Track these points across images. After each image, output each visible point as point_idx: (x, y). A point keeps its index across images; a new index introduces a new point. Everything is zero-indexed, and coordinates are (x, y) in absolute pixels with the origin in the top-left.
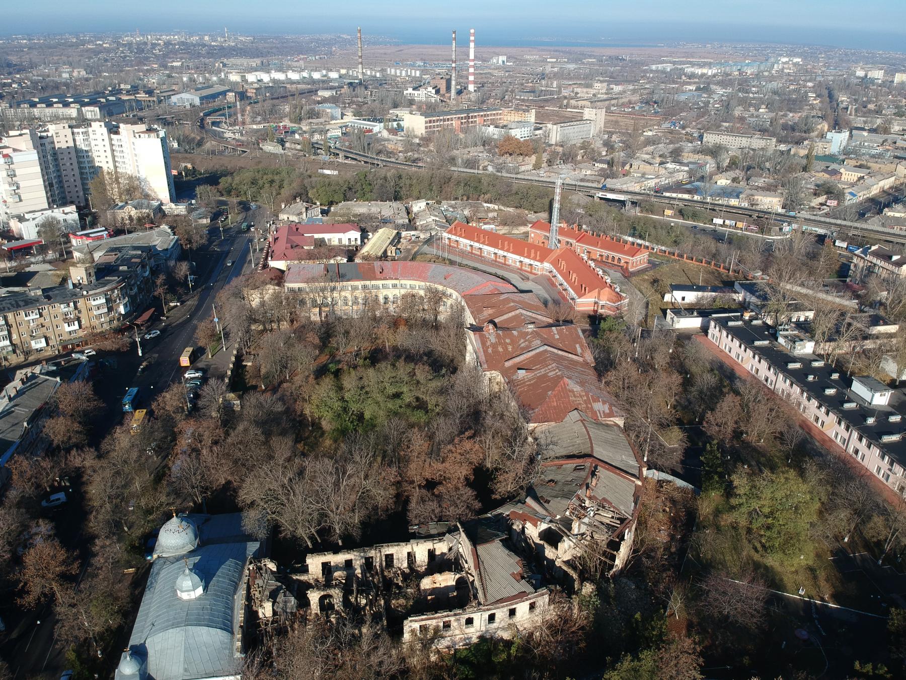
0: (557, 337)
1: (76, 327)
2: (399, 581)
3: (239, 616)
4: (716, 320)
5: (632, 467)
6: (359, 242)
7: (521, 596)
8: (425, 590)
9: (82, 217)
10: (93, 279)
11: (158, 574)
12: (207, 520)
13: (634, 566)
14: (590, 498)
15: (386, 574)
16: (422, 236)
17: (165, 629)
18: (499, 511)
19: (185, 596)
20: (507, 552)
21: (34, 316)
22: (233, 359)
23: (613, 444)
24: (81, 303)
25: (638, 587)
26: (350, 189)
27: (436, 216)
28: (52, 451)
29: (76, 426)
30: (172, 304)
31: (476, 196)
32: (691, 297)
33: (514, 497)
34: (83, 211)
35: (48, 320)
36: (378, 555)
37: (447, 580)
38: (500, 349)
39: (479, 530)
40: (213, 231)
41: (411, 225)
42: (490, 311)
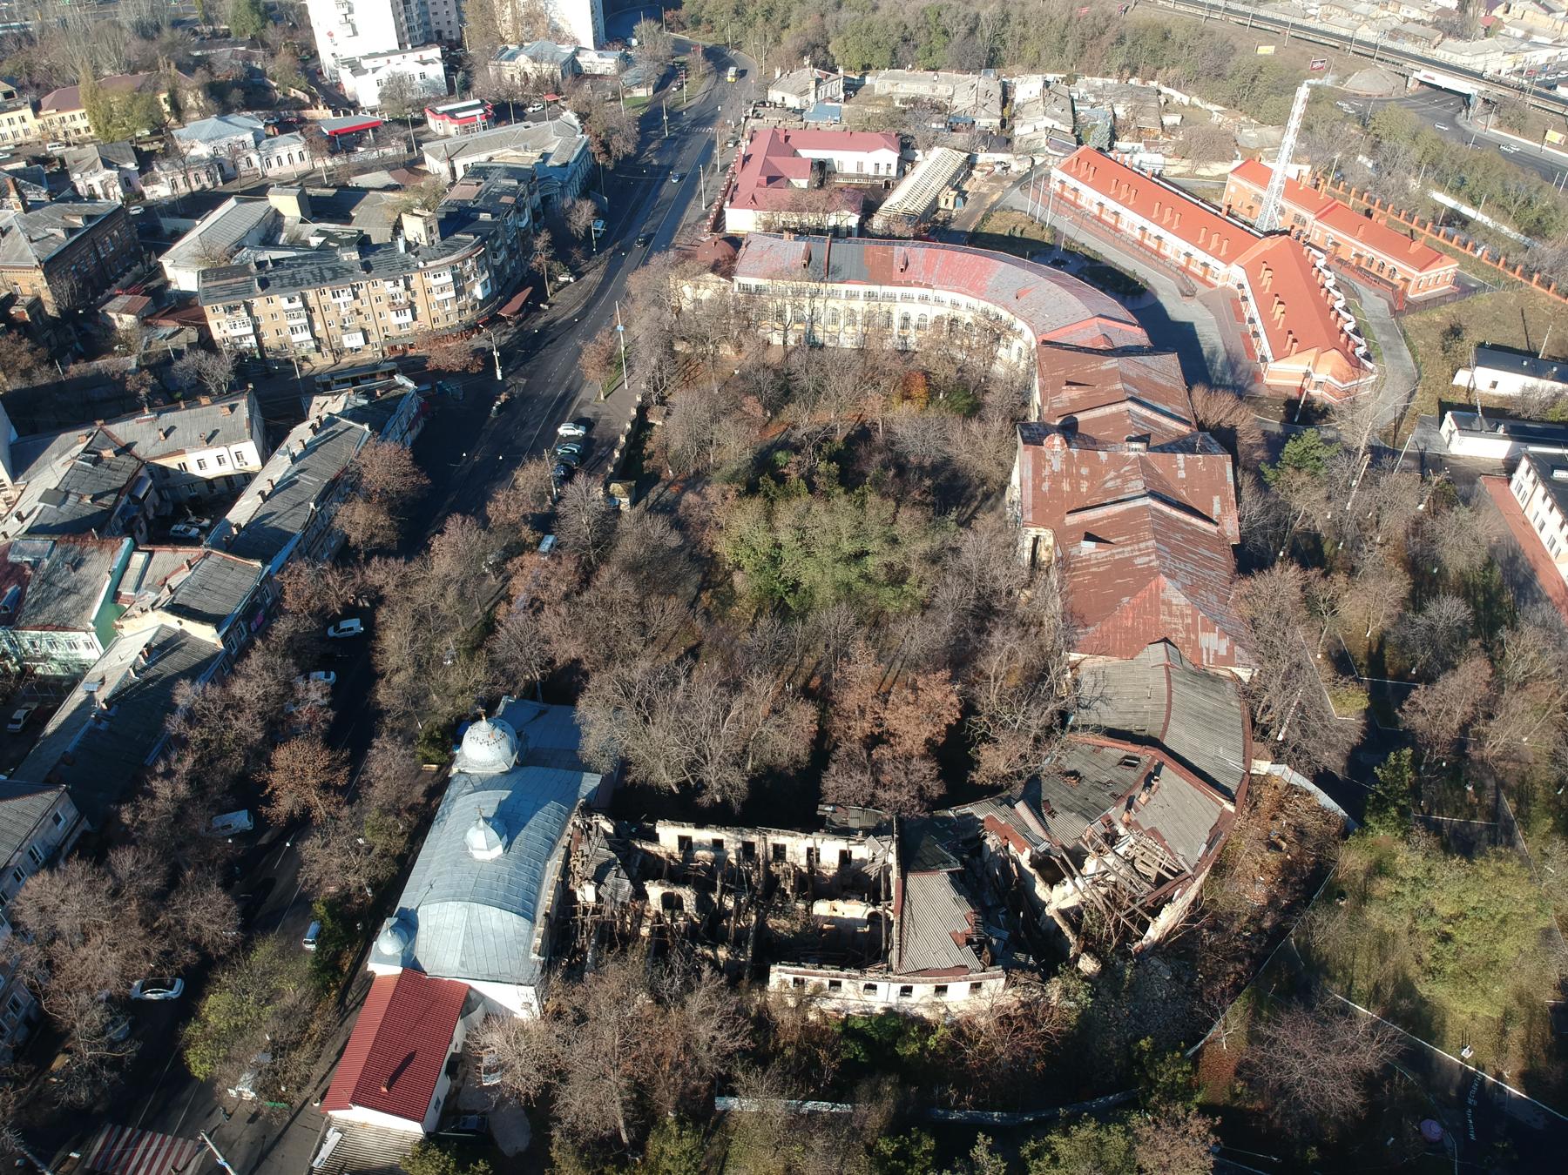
0: (1182, 474)
1: (409, 318)
2: (788, 886)
4: (1536, 460)
5: (1230, 773)
6: (893, 172)
7: (960, 970)
8: (818, 917)
9: (450, 70)
10: (436, 237)
11: (454, 800)
12: (542, 713)
13: (1179, 947)
14: (1127, 825)
15: (772, 868)
16: (1015, 167)
17: (444, 899)
18: (969, 809)
19: (478, 855)
20: (954, 894)
21: (346, 297)
22: (634, 412)
23: (1208, 721)
24: (415, 282)
25: (1177, 977)
26: (905, 40)
27: (1055, 117)
28: (346, 556)
29: (382, 519)
30: (561, 279)
31: (1150, 69)
32: (1508, 384)
33: (1000, 789)
34: (454, 62)
35: (367, 304)
36: (765, 841)
37: (854, 910)
38: (1066, 487)
39: (924, 842)
40: (649, 120)
41: (1002, 139)
42: (1075, 393)
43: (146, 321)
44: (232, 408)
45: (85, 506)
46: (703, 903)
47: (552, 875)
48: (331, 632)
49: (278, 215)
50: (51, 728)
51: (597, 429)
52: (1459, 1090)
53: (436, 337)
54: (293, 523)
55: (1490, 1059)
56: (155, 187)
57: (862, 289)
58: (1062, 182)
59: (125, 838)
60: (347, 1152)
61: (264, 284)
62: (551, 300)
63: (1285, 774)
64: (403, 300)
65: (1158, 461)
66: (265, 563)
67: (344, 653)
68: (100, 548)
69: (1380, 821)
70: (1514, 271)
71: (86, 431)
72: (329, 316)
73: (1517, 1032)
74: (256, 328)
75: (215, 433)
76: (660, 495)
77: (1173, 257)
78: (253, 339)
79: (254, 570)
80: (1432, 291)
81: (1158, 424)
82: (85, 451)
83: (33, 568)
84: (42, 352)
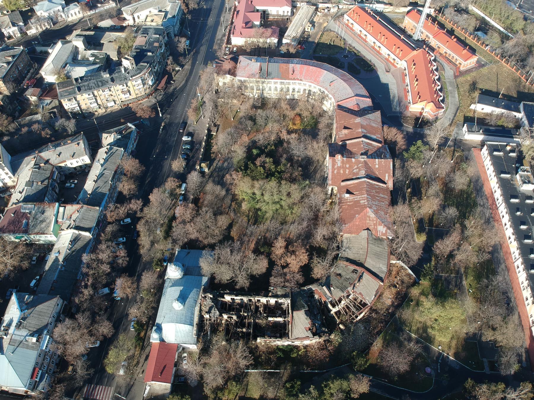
0: (377, 166)
2: (261, 309)
3: (196, 320)
5: (382, 272)
6: (289, 14)
10: (134, 66)
12: (189, 253)
13: (366, 321)
18: (310, 287)
20: (306, 317)
23: (378, 255)
24: (129, 84)
25: (365, 328)
36: (255, 299)
38: (342, 172)
39: (298, 300)
42: (346, 131)
43: (40, 98)
44: (78, 144)
45: (39, 186)
46: (239, 316)
47: (197, 313)
48: (122, 223)
49: (76, 48)
50: (47, 267)
51: (195, 137)
52: (436, 357)
53: (138, 99)
54: (105, 190)
55: (446, 349)
56: (31, 31)
57: (279, 81)
58: (348, 20)
59: (79, 309)
60: (152, 391)
61: (79, 89)
62: (174, 79)
63: (400, 263)
64: (126, 90)
65: (370, 161)
66: (100, 207)
67: (128, 233)
68: (49, 207)
69: (424, 279)
70: (497, 56)
71: (33, 156)
72: (102, 97)
73: (454, 343)
74: (79, 104)
75: (74, 153)
76: (217, 164)
77: (384, 54)
78: (78, 108)
79: (97, 210)
80: (469, 67)
81: (371, 144)
82: (35, 165)
83: (30, 214)
84: (10, 118)
